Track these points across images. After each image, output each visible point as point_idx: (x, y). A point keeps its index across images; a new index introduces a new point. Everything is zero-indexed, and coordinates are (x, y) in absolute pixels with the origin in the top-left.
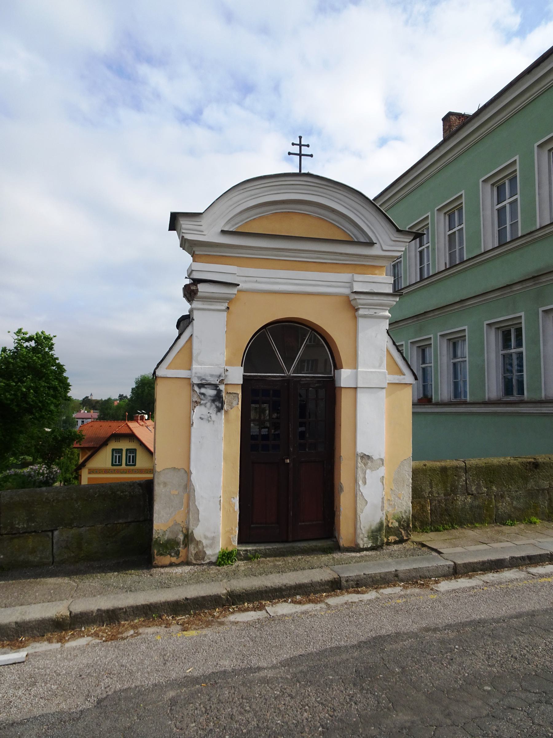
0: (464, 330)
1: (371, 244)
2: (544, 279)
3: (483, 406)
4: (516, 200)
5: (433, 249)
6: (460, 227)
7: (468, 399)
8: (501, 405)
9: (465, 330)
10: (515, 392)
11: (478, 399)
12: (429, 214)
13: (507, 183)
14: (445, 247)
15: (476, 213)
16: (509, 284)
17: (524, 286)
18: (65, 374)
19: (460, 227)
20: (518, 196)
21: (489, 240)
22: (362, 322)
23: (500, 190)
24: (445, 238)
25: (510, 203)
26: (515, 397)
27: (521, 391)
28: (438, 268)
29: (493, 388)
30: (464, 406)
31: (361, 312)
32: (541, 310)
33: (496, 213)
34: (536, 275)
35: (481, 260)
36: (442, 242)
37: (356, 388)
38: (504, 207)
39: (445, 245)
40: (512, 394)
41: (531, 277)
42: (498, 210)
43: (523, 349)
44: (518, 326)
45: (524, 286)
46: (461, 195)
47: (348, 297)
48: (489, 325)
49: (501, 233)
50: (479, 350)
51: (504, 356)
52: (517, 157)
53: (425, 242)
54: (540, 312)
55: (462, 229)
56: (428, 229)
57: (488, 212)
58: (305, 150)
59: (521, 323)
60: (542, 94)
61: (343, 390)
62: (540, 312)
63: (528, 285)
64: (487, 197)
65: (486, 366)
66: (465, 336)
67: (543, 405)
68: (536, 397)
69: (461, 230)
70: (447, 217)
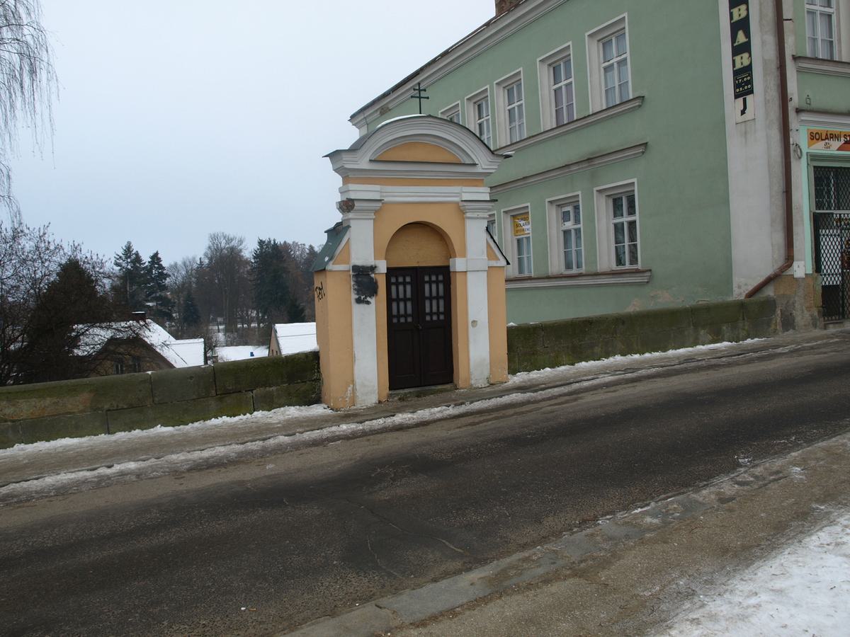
0: (633, 184)
1: (475, 165)
2: (597, 162)
3: (546, 280)
4: (571, 83)
5: (494, 123)
6: (519, 103)
7: (533, 275)
8: (563, 279)
9: (633, 183)
10: (574, 266)
11: (541, 273)
12: (488, 87)
13: (562, 64)
14: (505, 123)
15: (534, 91)
16: (567, 163)
17: (581, 166)
18: (249, 250)
19: (519, 103)
20: (572, 80)
21: (548, 121)
22: (469, 223)
23: (510, 92)
24: (505, 112)
25: (619, 63)
26: (574, 271)
27: (634, 259)
28: (544, 126)
29: (606, 260)
30: (529, 281)
31: (468, 215)
32: (502, 210)
33: (553, 93)
34: (592, 157)
35: (589, 121)
36: (502, 117)
37: (466, 272)
38: (561, 88)
39: (505, 119)
40: (572, 268)
41: (586, 158)
42: (509, 110)
43: (636, 217)
44: (576, 204)
45: (581, 166)
46: (520, 72)
47: (457, 203)
48: (551, 202)
49: (558, 112)
50: (541, 226)
51: (616, 225)
52: (521, 69)
53: (485, 115)
54: (595, 192)
55: (522, 105)
56: (458, 115)
57: (546, 91)
58: (423, 94)
59: (578, 201)
60: (402, 103)
61: (458, 275)
62: (595, 192)
63: (583, 166)
64: (544, 76)
65: (549, 244)
66: (528, 212)
67: (598, 277)
68: (593, 270)
69: (569, 85)
70: (506, 91)
